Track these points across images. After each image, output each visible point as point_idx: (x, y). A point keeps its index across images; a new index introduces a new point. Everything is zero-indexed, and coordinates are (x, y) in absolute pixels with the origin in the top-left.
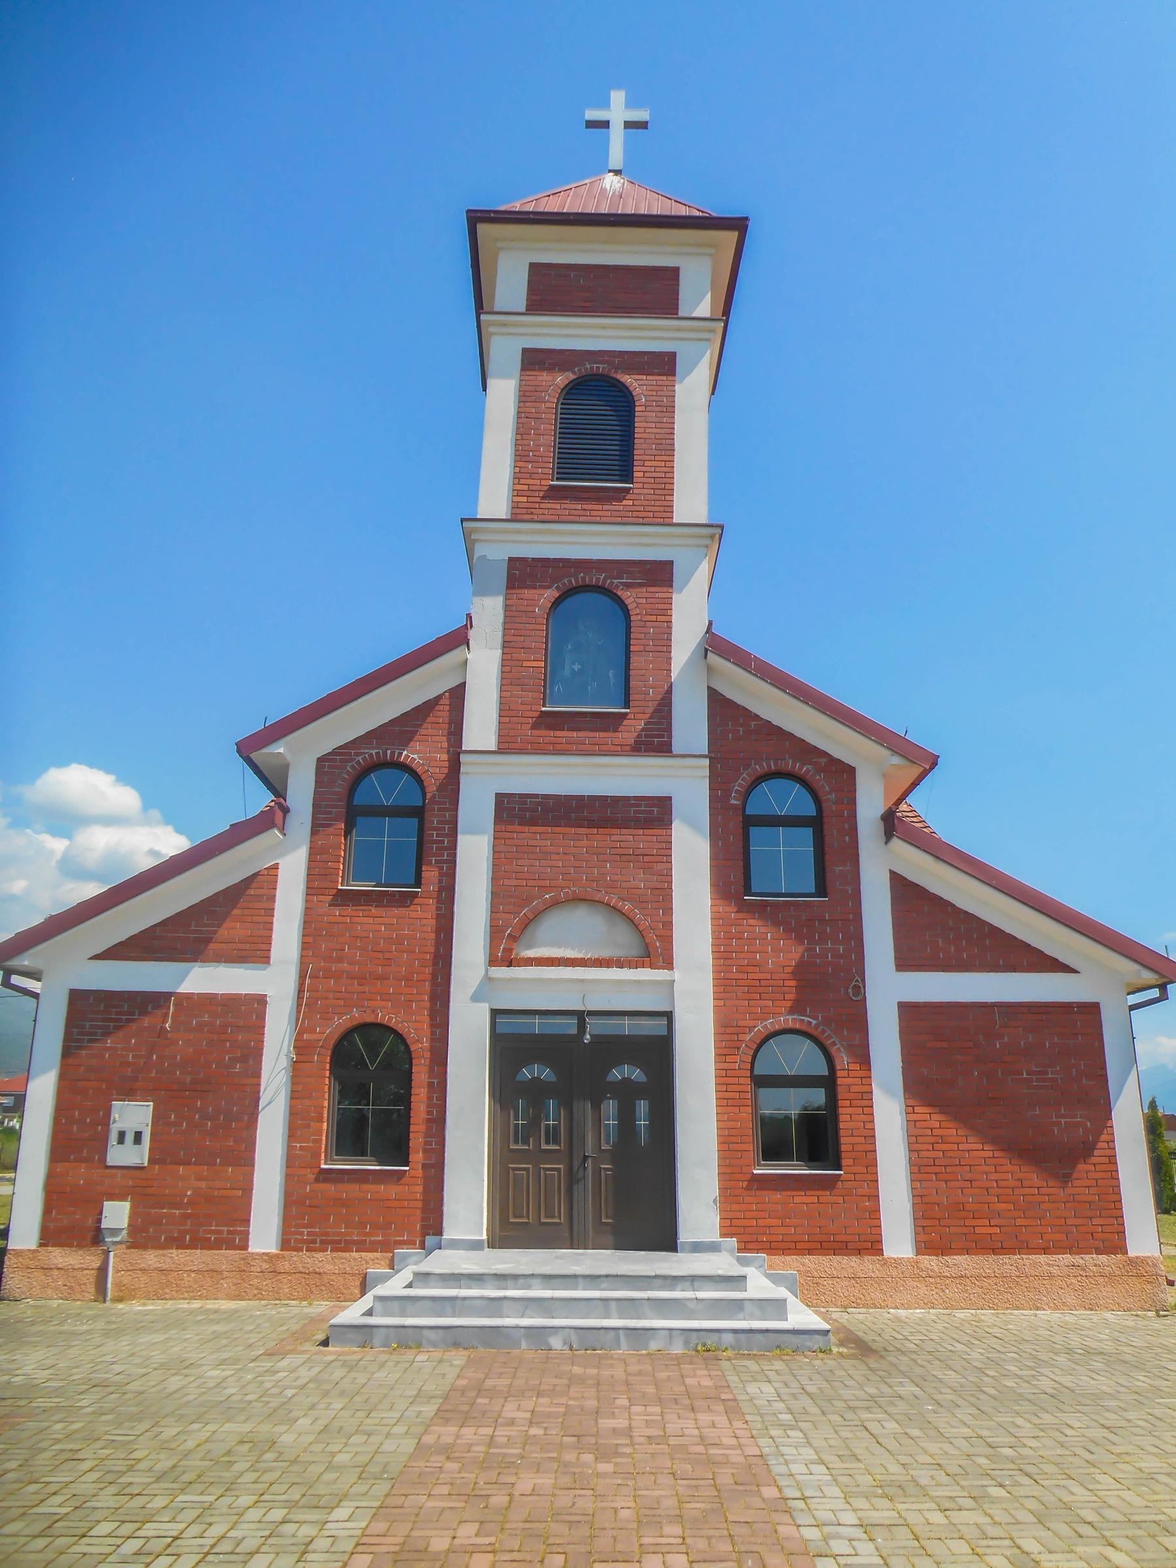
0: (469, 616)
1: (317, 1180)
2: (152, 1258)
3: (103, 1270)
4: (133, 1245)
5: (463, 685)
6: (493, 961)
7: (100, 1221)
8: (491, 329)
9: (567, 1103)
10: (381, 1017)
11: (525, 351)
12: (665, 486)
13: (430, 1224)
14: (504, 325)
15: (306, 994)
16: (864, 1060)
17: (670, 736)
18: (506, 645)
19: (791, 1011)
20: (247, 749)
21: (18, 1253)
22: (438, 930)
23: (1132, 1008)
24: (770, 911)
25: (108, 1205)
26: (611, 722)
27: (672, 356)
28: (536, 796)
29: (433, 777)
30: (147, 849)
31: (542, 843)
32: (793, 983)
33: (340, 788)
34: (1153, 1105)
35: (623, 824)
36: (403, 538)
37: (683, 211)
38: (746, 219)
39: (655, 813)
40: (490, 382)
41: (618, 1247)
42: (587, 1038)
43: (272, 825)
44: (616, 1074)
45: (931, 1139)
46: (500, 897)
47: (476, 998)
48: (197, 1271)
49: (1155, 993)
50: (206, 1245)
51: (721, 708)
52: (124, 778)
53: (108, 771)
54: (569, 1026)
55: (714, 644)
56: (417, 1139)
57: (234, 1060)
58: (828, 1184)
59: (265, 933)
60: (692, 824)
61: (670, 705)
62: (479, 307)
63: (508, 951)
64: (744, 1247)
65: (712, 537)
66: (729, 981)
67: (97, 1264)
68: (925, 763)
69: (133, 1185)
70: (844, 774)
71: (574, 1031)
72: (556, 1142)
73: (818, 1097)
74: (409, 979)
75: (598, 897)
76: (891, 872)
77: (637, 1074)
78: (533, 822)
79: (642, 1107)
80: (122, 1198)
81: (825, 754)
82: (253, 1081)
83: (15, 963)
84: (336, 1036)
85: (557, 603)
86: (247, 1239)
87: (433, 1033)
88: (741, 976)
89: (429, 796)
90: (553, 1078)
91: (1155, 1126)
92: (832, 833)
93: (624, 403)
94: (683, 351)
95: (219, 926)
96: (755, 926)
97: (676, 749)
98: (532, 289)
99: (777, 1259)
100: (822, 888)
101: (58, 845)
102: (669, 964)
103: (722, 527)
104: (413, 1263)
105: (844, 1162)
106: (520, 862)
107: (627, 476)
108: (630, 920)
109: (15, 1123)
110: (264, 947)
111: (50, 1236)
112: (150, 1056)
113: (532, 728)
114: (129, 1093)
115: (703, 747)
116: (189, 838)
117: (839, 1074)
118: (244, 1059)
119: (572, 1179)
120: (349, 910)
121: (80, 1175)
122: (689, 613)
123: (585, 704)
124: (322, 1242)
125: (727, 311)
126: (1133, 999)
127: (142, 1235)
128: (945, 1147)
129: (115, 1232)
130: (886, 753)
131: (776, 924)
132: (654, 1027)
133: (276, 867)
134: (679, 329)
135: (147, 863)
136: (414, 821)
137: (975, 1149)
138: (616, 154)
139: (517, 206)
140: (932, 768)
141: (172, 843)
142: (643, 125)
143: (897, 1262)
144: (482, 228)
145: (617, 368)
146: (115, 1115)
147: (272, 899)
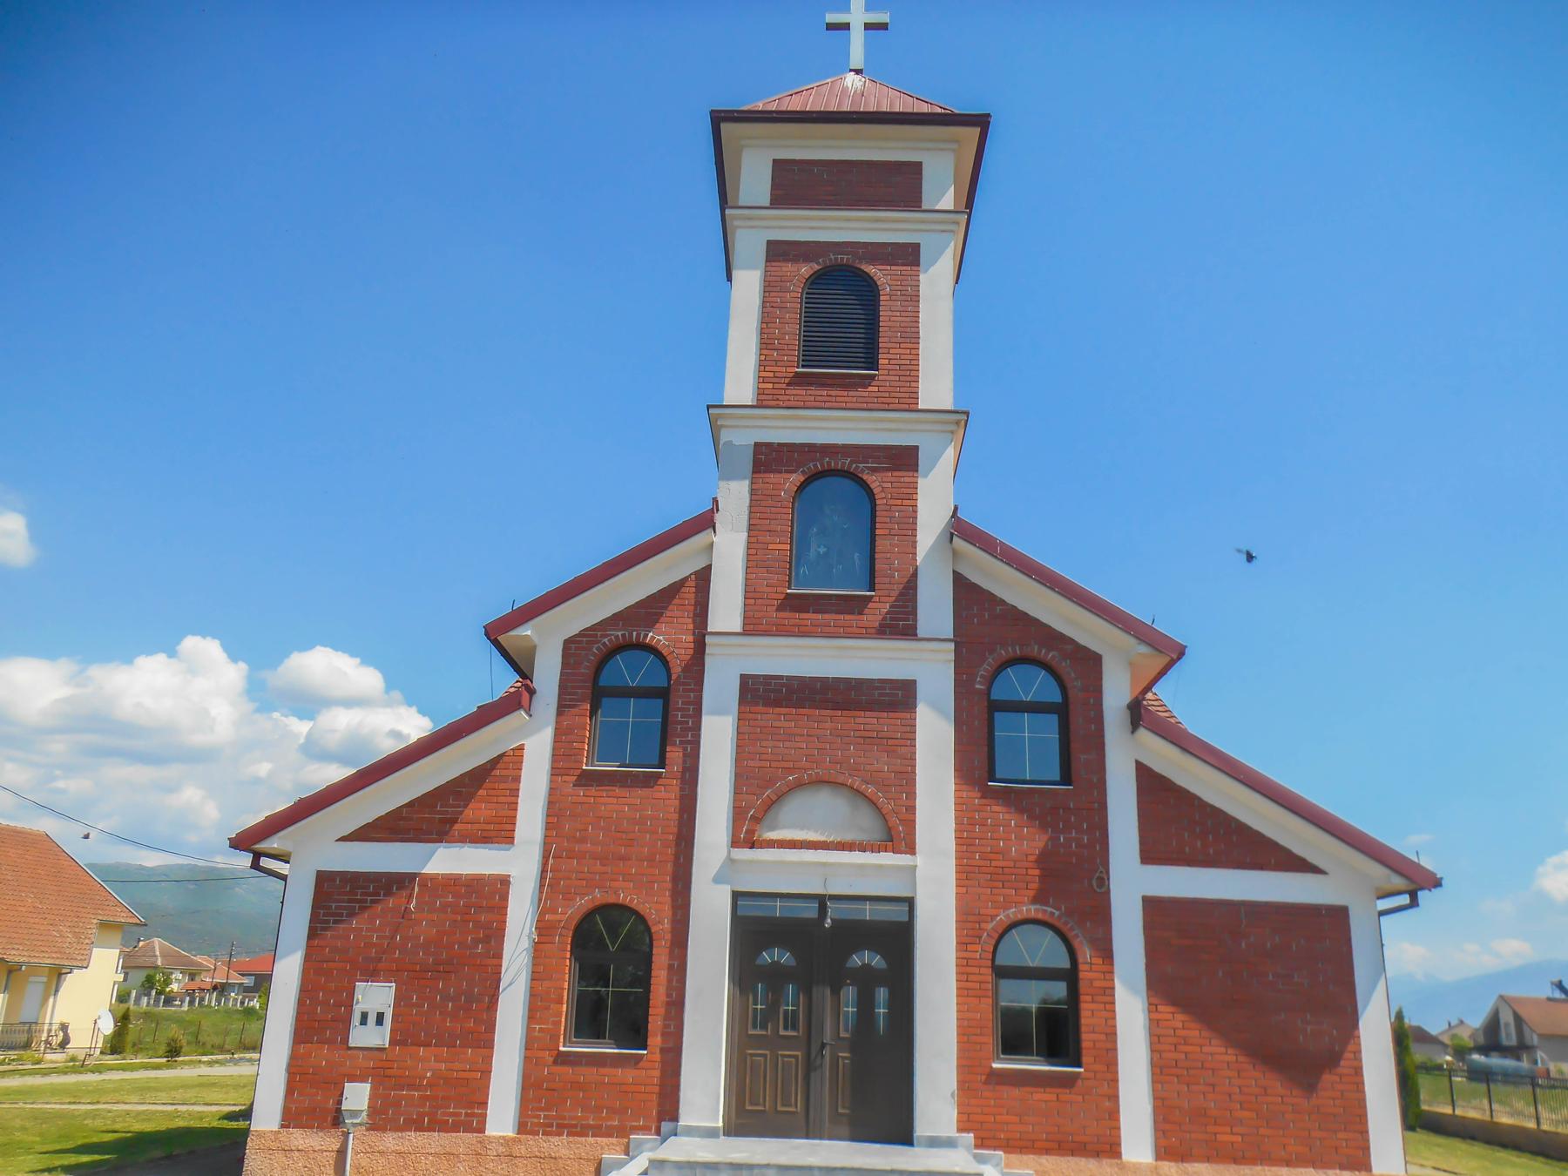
0: (715, 501)
1: (555, 1063)
2: (390, 1141)
3: (342, 1153)
4: (373, 1127)
5: (709, 567)
6: (735, 843)
7: (340, 1103)
8: (736, 223)
9: (806, 989)
10: (623, 898)
11: (769, 242)
12: (909, 373)
13: (666, 1110)
14: (750, 218)
15: (549, 875)
16: (1106, 953)
17: (915, 620)
18: (751, 528)
19: (1035, 900)
20: (495, 633)
21: (261, 1135)
22: (681, 824)
23: (1382, 913)
24: (1014, 798)
25: (349, 1088)
26: (853, 605)
27: (916, 247)
28: (780, 677)
29: (679, 655)
30: (387, 729)
31: (786, 724)
32: (1037, 872)
33: (586, 669)
34: (1400, 1016)
35: (870, 706)
36: (643, 423)
37: (925, 108)
38: (988, 115)
39: (898, 698)
40: (736, 274)
41: (855, 1138)
42: (828, 923)
43: (519, 706)
44: (856, 960)
45: (1175, 1040)
46: (743, 779)
47: (717, 880)
48: (435, 1154)
49: (1405, 899)
50: (444, 1127)
51: (966, 593)
52: (367, 660)
53: (353, 654)
54: (810, 911)
55: (959, 529)
56: (656, 1022)
57: (476, 941)
58: (1068, 1082)
59: (510, 813)
60: (936, 707)
61: (915, 588)
62: (724, 199)
63: (751, 832)
64: (981, 1143)
65: (958, 423)
66: (976, 866)
67: (336, 1146)
68: (1172, 653)
69: (377, 1068)
70: (1090, 663)
71: (814, 914)
72: (795, 1027)
73: (1059, 990)
74: (651, 859)
75: (841, 779)
76: (1137, 762)
77: (877, 961)
78: (777, 703)
79: (882, 994)
80: (361, 1079)
81: (1072, 641)
82: (495, 961)
83: (262, 846)
84: (577, 918)
85: (802, 487)
86: (484, 1122)
87: (674, 914)
88: (982, 863)
89: (674, 677)
90: (793, 963)
91: (1404, 1037)
92: (1077, 721)
93: (868, 293)
94: (926, 242)
95: (466, 806)
96: (999, 812)
97: (921, 633)
98: (776, 185)
99: (1014, 1158)
100: (1066, 778)
101: (302, 728)
102: (911, 850)
103: (967, 413)
104: (648, 1151)
105: (1084, 1059)
106: (764, 744)
107: (873, 364)
108: (872, 802)
109: (255, 1003)
110: (508, 827)
111: (291, 1118)
112: (393, 937)
113: (778, 610)
114: (372, 975)
115: (948, 630)
116: (432, 720)
117: (1081, 967)
118: (486, 940)
119: (810, 1067)
120: (593, 791)
121: (322, 1056)
122: (935, 498)
123: (831, 587)
124: (559, 1126)
125: (970, 204)
126: (1383, 905)
127: (381, 1118)
128: (1189, 1048)
129: (355, 1113)
130: (1133, 641)
131: (1021, 811)
132: (896, 913)
133: (521, 748)
134: (923, 222)
135: (389, 747)
136: (660, 702)
137: (1218, 1052)
138: (857, 57)
139: (760, 106)
140: (1179, 659)
141: (415, 726)
142: (883, 27)
143: (1136, 1168)
144: (725, 128)
145: (861, 259)
146: (358, 996)
147: (517, 779)
